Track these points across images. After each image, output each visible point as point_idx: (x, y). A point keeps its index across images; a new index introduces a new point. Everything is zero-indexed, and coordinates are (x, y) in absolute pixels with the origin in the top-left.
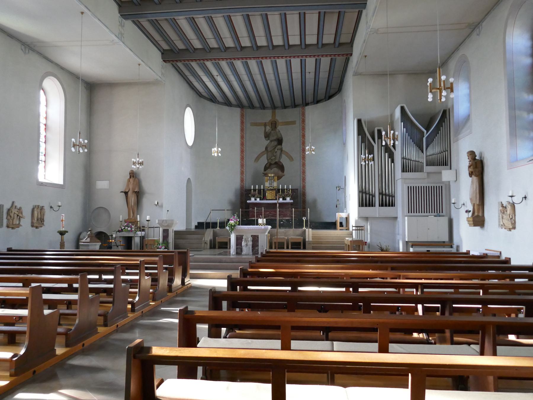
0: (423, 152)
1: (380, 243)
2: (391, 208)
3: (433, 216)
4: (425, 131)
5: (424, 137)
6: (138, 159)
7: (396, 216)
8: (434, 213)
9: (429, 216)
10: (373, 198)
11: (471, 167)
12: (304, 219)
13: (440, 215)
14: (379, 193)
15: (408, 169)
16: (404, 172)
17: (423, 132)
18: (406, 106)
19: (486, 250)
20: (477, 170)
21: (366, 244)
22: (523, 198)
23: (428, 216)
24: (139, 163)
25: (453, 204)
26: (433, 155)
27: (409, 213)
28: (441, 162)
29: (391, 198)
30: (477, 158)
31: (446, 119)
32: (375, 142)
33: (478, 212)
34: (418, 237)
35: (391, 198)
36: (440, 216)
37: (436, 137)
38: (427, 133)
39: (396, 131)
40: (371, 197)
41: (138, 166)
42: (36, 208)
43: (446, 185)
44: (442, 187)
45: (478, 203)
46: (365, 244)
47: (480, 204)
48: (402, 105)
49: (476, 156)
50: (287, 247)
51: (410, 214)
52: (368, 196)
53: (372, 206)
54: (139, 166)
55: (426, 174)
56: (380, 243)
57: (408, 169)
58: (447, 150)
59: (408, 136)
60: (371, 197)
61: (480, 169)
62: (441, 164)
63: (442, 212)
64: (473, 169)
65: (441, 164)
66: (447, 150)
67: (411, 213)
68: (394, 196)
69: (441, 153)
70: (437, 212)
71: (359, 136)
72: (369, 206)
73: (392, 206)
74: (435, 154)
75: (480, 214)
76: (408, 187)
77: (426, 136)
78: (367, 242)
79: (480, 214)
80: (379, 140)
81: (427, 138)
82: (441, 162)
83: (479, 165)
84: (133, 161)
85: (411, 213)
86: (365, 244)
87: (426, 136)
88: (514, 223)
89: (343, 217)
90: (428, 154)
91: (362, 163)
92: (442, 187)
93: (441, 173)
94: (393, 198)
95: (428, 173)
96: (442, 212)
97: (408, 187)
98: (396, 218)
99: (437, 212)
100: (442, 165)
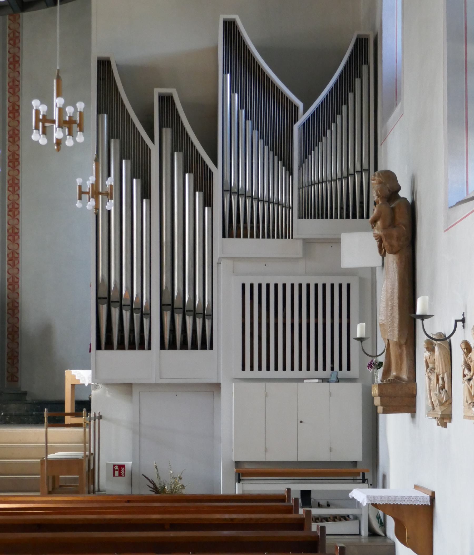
0: (291, 173)
1: (156, 467)
2: (199, 353)
3: (317, 381)
4: (300, 105)
5: (296, 119)
6: (58, 102)
7: (215, 381)
8: (324, 369)
9: (305, 381)
10: (145, 320)
11: (379, 223)
12: (375, 391)
13: (339, 377)
14: (162, 306)
15: (245, 228)
16: (231, 236)
17: (296, 109)
18: (240, 17)
19: (416, 487)
20: (395, 232)
21: (122, 472)
22: (456, 321)
23: (301, 380)
24: (65, 122)
25: (358, 342)
26: (322, 183)
27: (244, 369)
28: (342, 208)
29: (199, 322)
30: (402, 194)
31: (365, 68)
32: (153, 140)
33: (399, 369)
34: (331, 450)
35: (199, 322)
36: (338, 381)
37: (333, 125)
38: (305, 111)
39: (52, 119)
40: (136, 316)
41: (58, 134)
42: (393, 321)
43: (362, 281)
44: (349, 286)
45: (395, 340)
46: (120, 470)
47: (403, 342)
48: (230, 17)
49: (399, 188)
50: (281, 502)
51: (248, 373)
52: (126, 315)
53: (142, 347)
54: (65, 137)
55: (299, 245)
56: (156, 467)
57: (245, 228)
58: (367, 168)
59: (110, 137)
60: (136, 316)
61: (404, 229)
62: (336, 212)
63: (349, 369)
64: (384, 228)
65: (336, 212)
66: (365, 166)
67: (276, 369)
68: (211, 316)
69: (348, 174)
70: (332, 369)
71: (100, 116)
72: (132, 347)
73: (204, 347)
74: (329, 178)
75: (404, 376)
76: (243, 286)
77: (303, 118)
78: (124, 466)
79: (404, 376)
80: (164, 130)
81: (306, 125)
82: (342, 208)
83: (402, 219)
84: (37, 112)
85: (292, 369)
86: (120, 470)
87: (303, 118)
88: (446, 401)
89: (81, 382)
90: (307, 179)
91: (108, 208)
92: (349, 286)
93: (337, 241)
94: (208, 322)
95: (307, 242)
96: (349, 369)
97: (243, 286)
98: (218, 386)
99: (332, 369)
100: (351, 216)
